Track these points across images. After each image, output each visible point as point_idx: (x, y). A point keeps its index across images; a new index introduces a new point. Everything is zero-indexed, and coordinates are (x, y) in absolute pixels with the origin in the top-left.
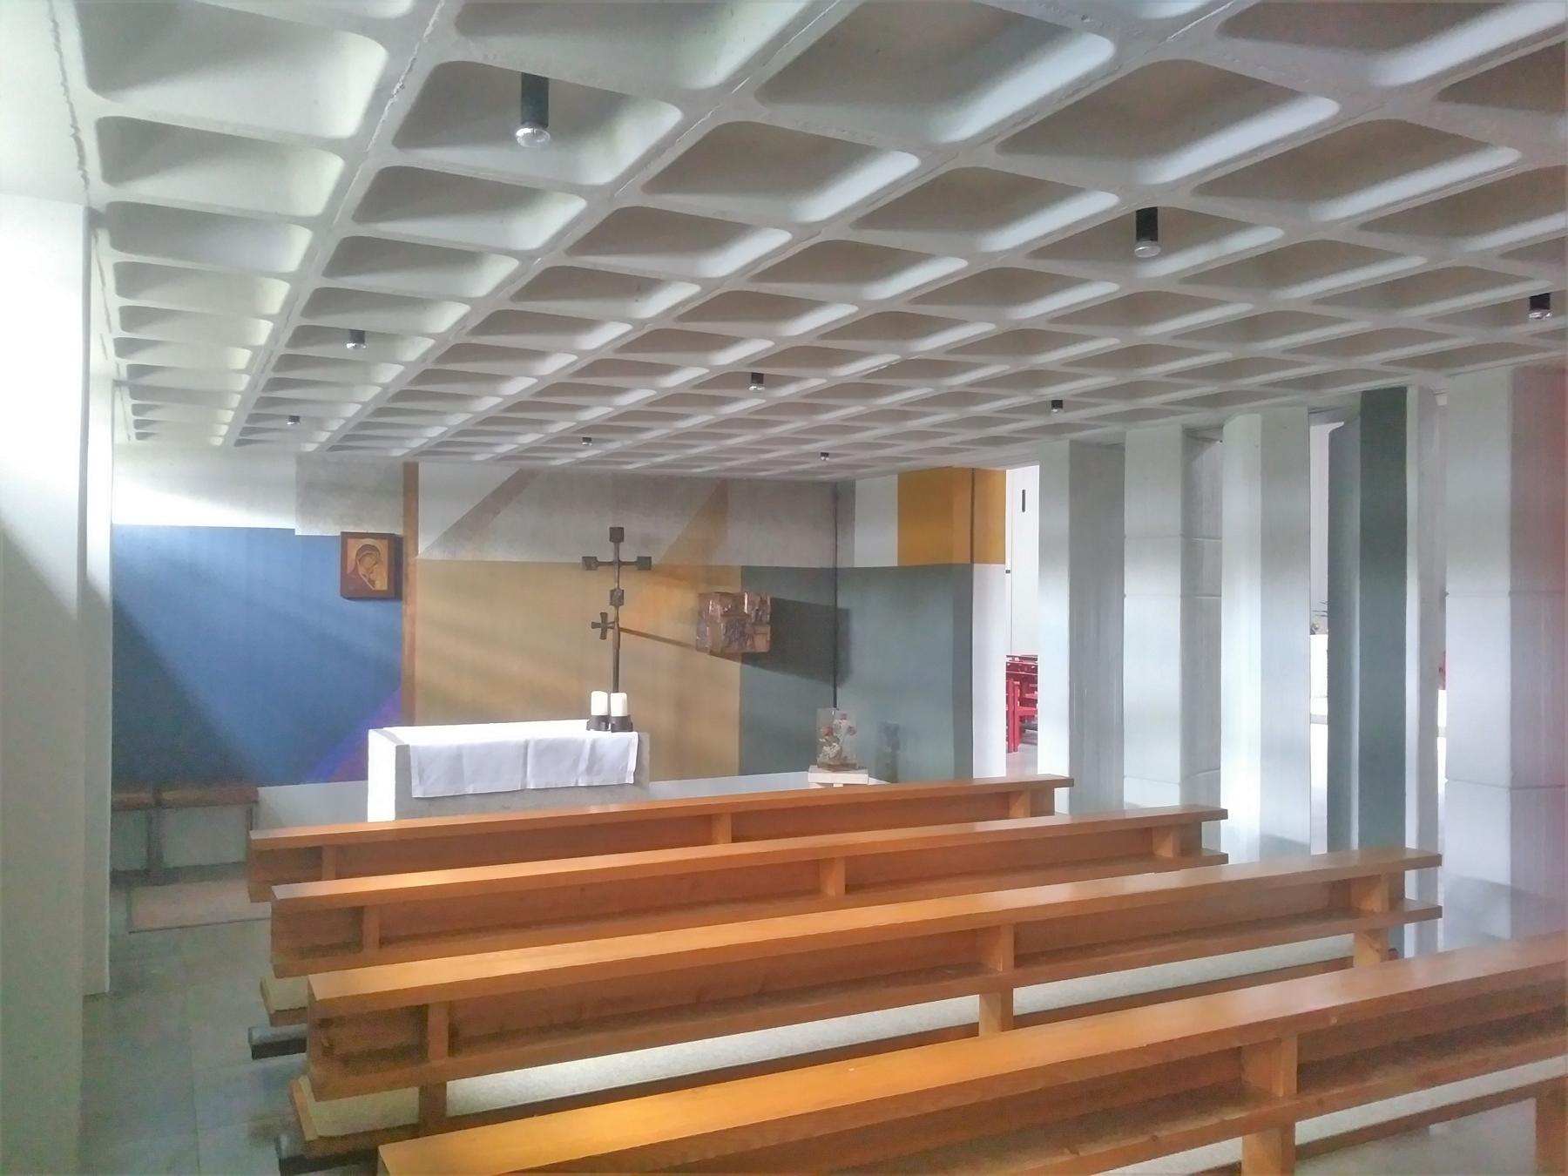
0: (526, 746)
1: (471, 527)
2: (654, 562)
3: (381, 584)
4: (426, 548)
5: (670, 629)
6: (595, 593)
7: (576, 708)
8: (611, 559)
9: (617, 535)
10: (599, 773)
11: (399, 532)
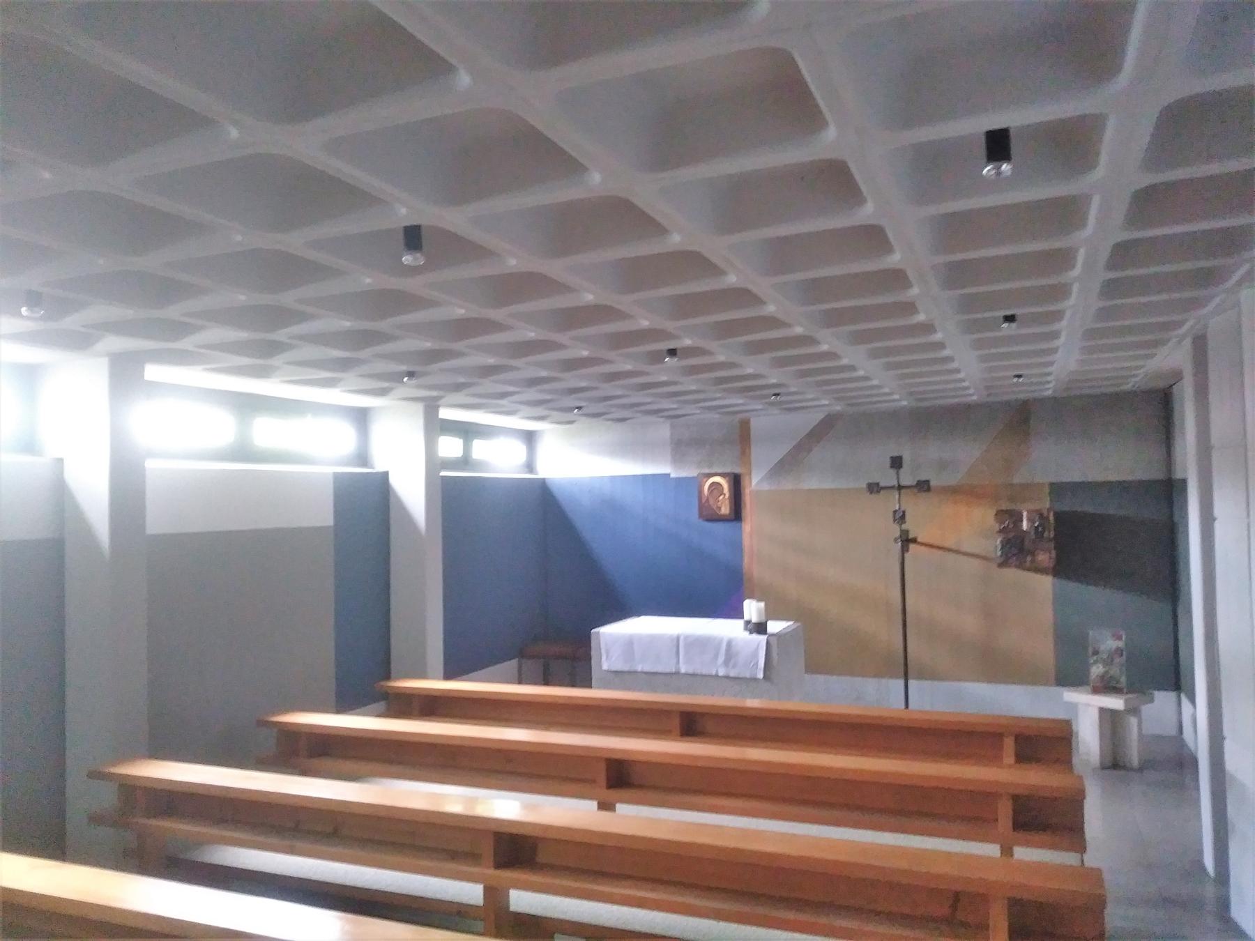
0: (678, 638)
1: (784, 467)
2: (933, 483)
3: (725, 510)
4: (755, 482)
5: (972, 544)
6: (879, 512)
7: (737, 613)
8: (895, 483)
9: (897, 463)
10: (734, 666)
11: (737, 470)
